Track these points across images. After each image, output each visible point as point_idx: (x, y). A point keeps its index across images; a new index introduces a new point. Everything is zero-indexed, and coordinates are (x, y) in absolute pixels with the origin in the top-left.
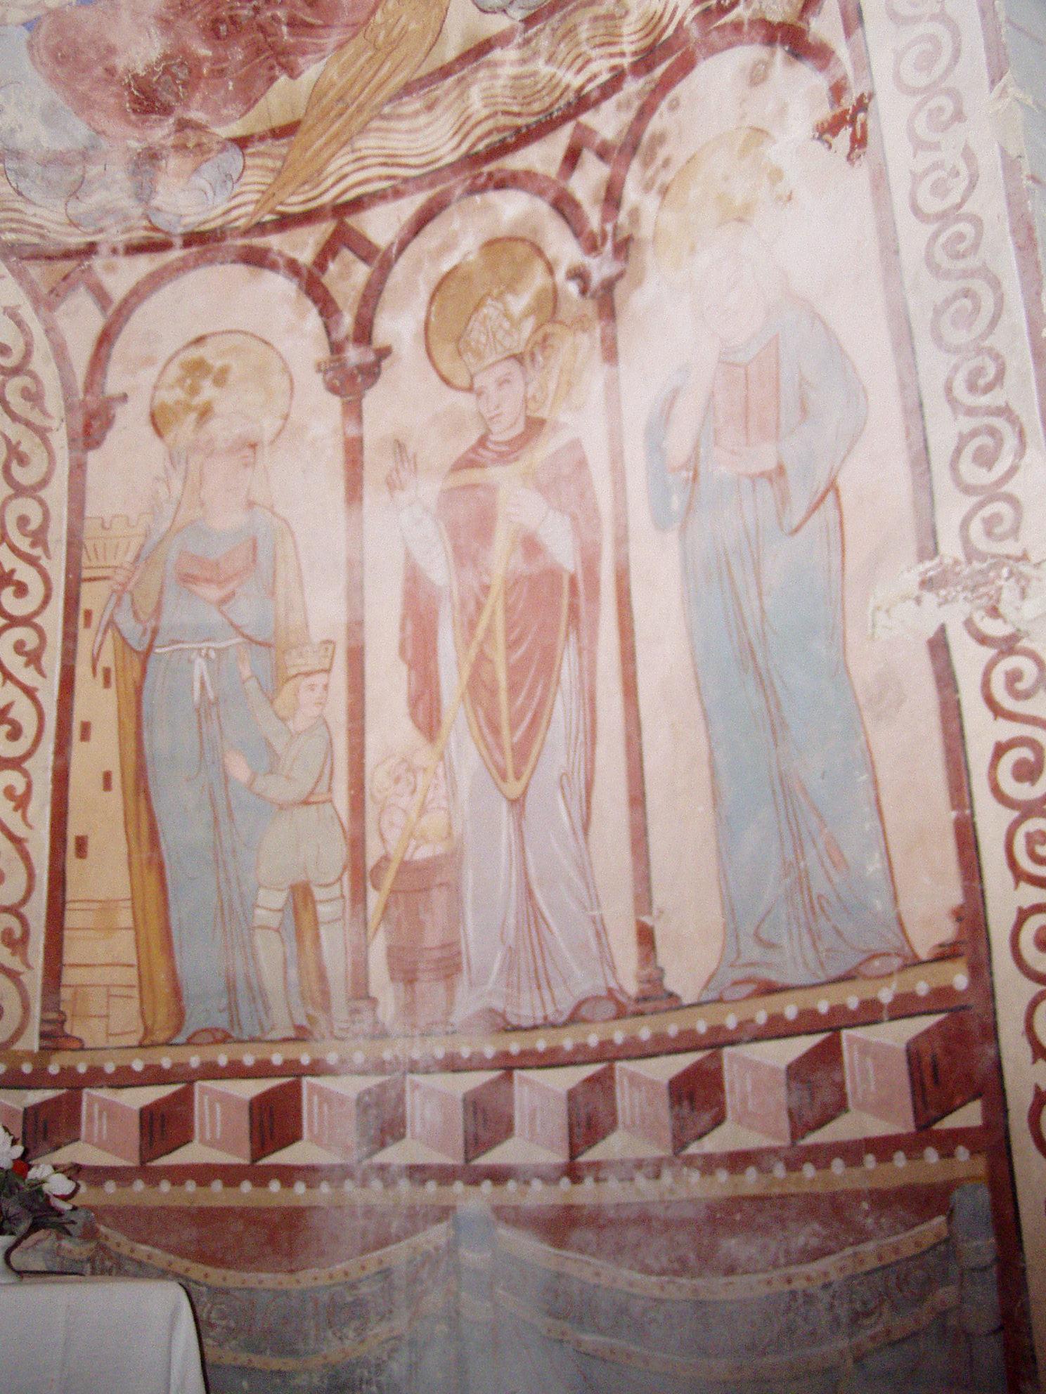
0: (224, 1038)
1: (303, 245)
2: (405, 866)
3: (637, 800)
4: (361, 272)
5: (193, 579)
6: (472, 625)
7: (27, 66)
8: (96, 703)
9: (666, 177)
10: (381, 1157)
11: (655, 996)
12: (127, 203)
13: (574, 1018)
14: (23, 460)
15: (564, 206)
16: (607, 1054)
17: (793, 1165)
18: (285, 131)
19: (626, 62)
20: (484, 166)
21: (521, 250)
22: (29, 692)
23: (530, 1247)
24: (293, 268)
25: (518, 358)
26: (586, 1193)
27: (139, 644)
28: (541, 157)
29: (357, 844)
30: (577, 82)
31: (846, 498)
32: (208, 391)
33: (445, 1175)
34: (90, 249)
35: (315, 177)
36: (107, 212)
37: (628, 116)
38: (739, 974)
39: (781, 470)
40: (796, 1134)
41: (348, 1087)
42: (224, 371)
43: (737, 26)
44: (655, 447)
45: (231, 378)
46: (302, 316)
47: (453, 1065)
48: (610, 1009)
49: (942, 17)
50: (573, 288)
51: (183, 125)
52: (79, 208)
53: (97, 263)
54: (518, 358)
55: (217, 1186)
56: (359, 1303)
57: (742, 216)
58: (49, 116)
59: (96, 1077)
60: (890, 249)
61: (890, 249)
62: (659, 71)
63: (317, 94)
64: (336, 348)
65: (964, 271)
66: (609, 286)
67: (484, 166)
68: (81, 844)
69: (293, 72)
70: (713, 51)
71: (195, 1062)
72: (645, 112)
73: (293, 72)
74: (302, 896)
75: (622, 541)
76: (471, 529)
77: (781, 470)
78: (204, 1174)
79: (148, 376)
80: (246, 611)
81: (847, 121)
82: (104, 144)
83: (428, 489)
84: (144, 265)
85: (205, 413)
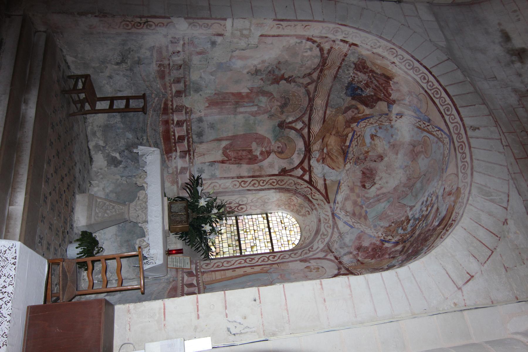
8: (257, 269)
12: (342, 254)
22: (257, 261)
36: (340, 252)
51: (358, 254)
53: (331, 254)
65: (66, 220)
79: (315, 264)
84: (333, 258)
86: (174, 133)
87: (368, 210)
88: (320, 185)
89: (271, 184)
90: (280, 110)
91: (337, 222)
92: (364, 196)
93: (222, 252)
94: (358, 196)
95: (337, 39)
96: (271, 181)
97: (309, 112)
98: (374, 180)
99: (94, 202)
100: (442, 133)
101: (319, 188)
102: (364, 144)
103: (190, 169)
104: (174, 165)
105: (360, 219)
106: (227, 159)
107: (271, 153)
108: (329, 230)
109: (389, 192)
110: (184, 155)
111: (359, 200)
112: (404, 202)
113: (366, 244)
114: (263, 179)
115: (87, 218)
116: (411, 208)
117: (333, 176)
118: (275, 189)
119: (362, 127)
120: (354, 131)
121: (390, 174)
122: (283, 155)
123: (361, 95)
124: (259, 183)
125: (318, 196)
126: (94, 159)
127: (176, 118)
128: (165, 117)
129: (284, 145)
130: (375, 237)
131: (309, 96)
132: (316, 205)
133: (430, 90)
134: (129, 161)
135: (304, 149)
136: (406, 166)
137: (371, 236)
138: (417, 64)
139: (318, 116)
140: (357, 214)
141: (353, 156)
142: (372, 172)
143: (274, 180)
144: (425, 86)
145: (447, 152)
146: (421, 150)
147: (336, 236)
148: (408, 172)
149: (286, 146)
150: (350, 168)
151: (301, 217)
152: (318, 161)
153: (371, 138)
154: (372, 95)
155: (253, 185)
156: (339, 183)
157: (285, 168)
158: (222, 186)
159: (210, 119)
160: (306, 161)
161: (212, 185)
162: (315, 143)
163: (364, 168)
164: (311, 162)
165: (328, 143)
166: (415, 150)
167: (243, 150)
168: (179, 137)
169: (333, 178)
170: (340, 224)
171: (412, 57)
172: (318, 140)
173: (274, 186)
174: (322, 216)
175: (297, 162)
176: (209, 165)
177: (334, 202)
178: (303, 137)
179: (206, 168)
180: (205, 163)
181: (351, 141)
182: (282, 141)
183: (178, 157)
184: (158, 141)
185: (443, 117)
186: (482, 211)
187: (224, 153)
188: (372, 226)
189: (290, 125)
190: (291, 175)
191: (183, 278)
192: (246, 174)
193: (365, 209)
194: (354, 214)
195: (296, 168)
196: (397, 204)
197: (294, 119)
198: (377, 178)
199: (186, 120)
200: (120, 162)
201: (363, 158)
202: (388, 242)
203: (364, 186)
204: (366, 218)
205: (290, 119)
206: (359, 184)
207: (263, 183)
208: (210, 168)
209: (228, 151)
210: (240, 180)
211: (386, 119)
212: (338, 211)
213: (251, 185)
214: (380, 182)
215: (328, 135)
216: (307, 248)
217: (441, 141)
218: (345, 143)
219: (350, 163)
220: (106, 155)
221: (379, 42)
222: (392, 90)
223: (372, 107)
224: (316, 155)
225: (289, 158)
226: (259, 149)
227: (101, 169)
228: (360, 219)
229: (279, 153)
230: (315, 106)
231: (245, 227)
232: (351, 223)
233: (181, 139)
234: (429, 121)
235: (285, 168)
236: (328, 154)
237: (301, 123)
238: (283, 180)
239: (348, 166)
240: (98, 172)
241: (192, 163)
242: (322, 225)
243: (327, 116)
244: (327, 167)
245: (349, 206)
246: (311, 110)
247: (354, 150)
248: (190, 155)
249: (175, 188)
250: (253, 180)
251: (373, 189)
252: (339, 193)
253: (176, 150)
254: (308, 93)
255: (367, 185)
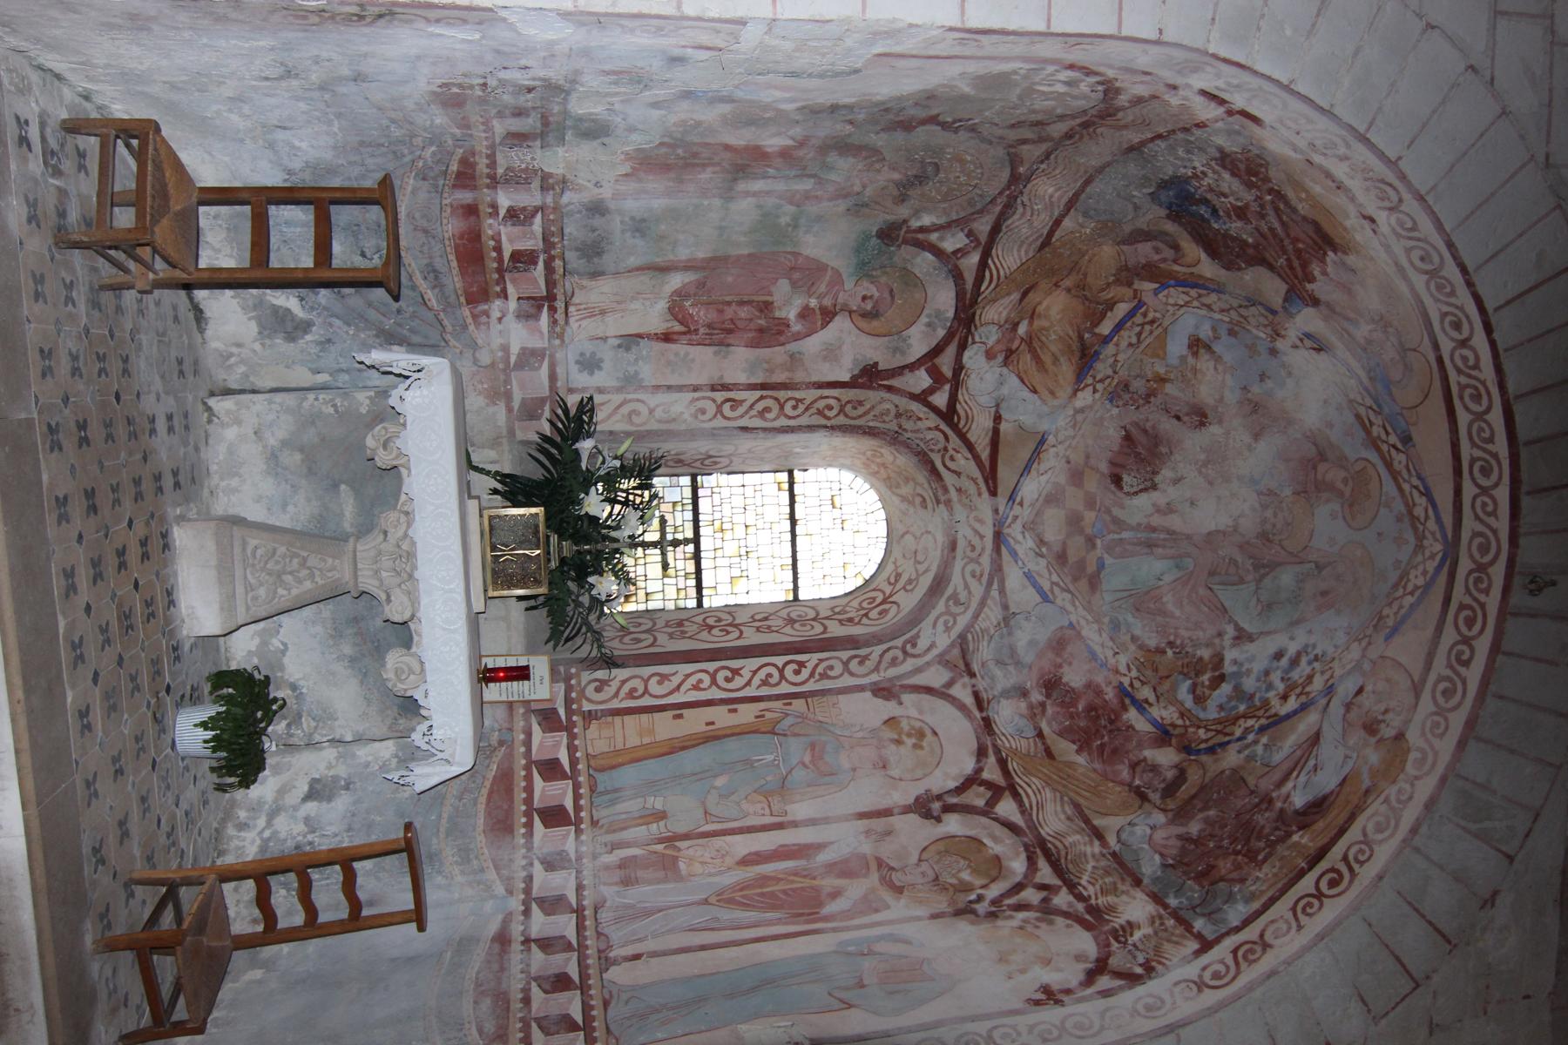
0: (592, 791)
1: (991, 773)
2: (675, 859)
3: (703, 948)
4: (980, 803)
5: (813, 749)
6: (796, 874)
7: (1053, 628)
8: (747, 713)
9: (1029, 928)
10: (536, 863)
11: (606, 962)
12: (999, 688)
13: (599, 934)
14: (861, 663)
15: (1019, 887)
16: (582, 947)
17: (522, 1020)
18: (1049, 754)
19: (1093, 902)
20: (1039, 848)
21: (994, 873)
22: (749, 683)
23: (493, 927)
24: (979, 771)
25: (937, 878)
26: (516, 947)
27: (779, 728)
28: (1045, 874)
29: (686, 837)
30: (1083, 882)
31: (846, 1012)
32: (910, 742)
33: (528, 891)
34: (972, 675)
35: (1027, 772)
36: (993, 678)
37: (1065, 908)
38: (615, 993)
39: (863, 986)
40: (537, 1020)
41: (570, 845)
42: (921, 748)
43: (1108, 945)
44: (880, 938)
45: (919, 752)
46: (954, 779)
47: (580, 888)
48: (602, 947)
49: (1102, 1028)
50: (973, 897)
51: (1043, 705)
52: (991, 665)
53: (966, 679)
54: (937, 878)
55: (524, 795)
56: (469, 861)
57: (1002, 959)
58: (1032, 643)
59: (572, 737)
60: (974, 1019)
61: (974, 1019)
62: (1088, 917)
63: (1070, 764)
64: (939, 797)
66: (974, 912)
67: (1039, 848)
68: (680, 716)
69: (1078, 752)
70: (1095, 938)
71: (581, 779)
72: (1066, 915)
73: (1078, 752)
74: (661, 816)
75: (834, 930)
76: (845, 869)
77: (863, 986)
78: (529, 789)
79: (913, 713)
80: (799, 774)
81: (1050, 996)
82: (1025, 671)
83: (867, 848)
84: (969, 700)
85: (899, 742)
86: (499, 242)
87: (1109, 560)
88: (979, 431)
89: (820, 413)
90: (896, 193)
91: (1006, 568)
92: (1109, 512)
93: (641, 594)
94: (1090, 503)
95: (1188, 86)
96: (821, 404)
97: (998, 209)
98: (1155, 473)
99: (237, 550)
100: (1431, 512)
101: (972, 437)
102: (1159, 350)
103: (552, 357)
104: (497, 341)
105: (1075, 579)
106: (682, 329)
107: (835, 314)
108: (973, 584)
109: (1189, 537)
110: (533, 311)
111: (1090, 516)
112: (1226, 596)
113: (1074, 677)
114: (797, 394)
115: (222, 609)
116: (1242, 637)
117: (1025, 410)
118: (832, 428)
119: (1171, 301)
120: (1141, 304)
121: (1211, 483)
122: (875, 323)
123: (1208, 221)
124: (782, 407)
125: (964, 462)
126: (208, 314)
127: (504, 200)
128: (466, 197)
129: (886, 295)
130: (1104, 665)
131: (1013, 169)
132: (953, 493)
133: (1459, 371)
134: (337, 322)
135: (951, 314)
136: (1271, 493)
137: (1093, 656)
138: (1452, 272)
139: (1026, 227)
140: (1072, 559)
141: (1110, 372)
142: (1156, 445)
143: (832, 402)
144: (1446, 346)
145: (1415, 579)
146: (1340, 485)
147: (993, 614)
148: (1269, 513)
149: (892, 296)
150: (1091, 407)
151: (896, 500)
152: (990, 355)
153: (1190, 347)
154: (1245, 242)
155: (761, 414)
156: (1042, 442)
157: (876, 364)
158: (658, 413)
159: (632, 206)
160: (951, 350)
161: (625, 410)
162: (995, 301)
163: (1136, 424)
164: (967, 354)
165: (1040, 309)
166: (1322, 468)
167: (741, 303)
168: (516, 256)
169: (1028, 420)
170: (1014, 577)
171: (1450, 245)
172: (1009, 294)
173: (829, 418)
174: (964, 532)
175: (918, 347)
176: (619, 346)
177: (1012, 498)
178: (957, 276)
179: (606, 353)
180: (604, 339)
181: (1119, 327)
182: (883, 279)
183: (510, 317)
184: (439, 264)
185: (1458, 472)
186: (1441, 868)
187: (675, 311)
188: (1106, 620)
189: (920, 236)
190: (890, 389)
191: (529, 734)
192: (742, 378)
193: (1099, 551)
194: (1062, 558)
195: (912, 367)
196: (1202, 591)
197: (942, 221)
198: (1166, 473)
199: (542, 208)
200: (306, 326)
201: (1142, 391)
202: (1141, 706)
203: (1117, 480)
204: (1094, 583)
205: (927, 220)
206: (1104, 467)
207: (795, 408)
208: (621, 353)
209: (687, 304)
210: (720, 396)
211: (1262, 320)
212: (1014, 531)
213: (753, 412)
214: (1171, 490)
215: (1044, 285)
216: (899, 642)
217: (1415, 530)
218: (1096, 324)
219: (1095, 391)
220: (250, 303)
221: (1348, 146)
222: (1325, 273)
223: (1228, 267)
224: (988, 333)
225: (896, 334)
226: (798, 302)
227: (239, 345)
228: (1075, 579)
229: (865, 315)
230: (1025, 199)
231: (717, 515)
232: (1046, 586)
233: (523, 259)
234: (1407, 439)
235: (876, 364)
236: (1029, 340)
237: (961, 235)
238: (861, 403)
239: (1085, 398)
240: (231, 355)
241: (561, 336)
242: (958, 565)
243: (1057, 234)
244: (1014, 381)
245: (1053, 534)
246: (1009, 207)
247: (1119, 357)
248: (553, 309)
249: (500, 413)
250: (762, 398)
251: (1143, 501)
252: (1033, 472)
253: (504, 295)
254: (1014, 161)
255: (1126, 478)
